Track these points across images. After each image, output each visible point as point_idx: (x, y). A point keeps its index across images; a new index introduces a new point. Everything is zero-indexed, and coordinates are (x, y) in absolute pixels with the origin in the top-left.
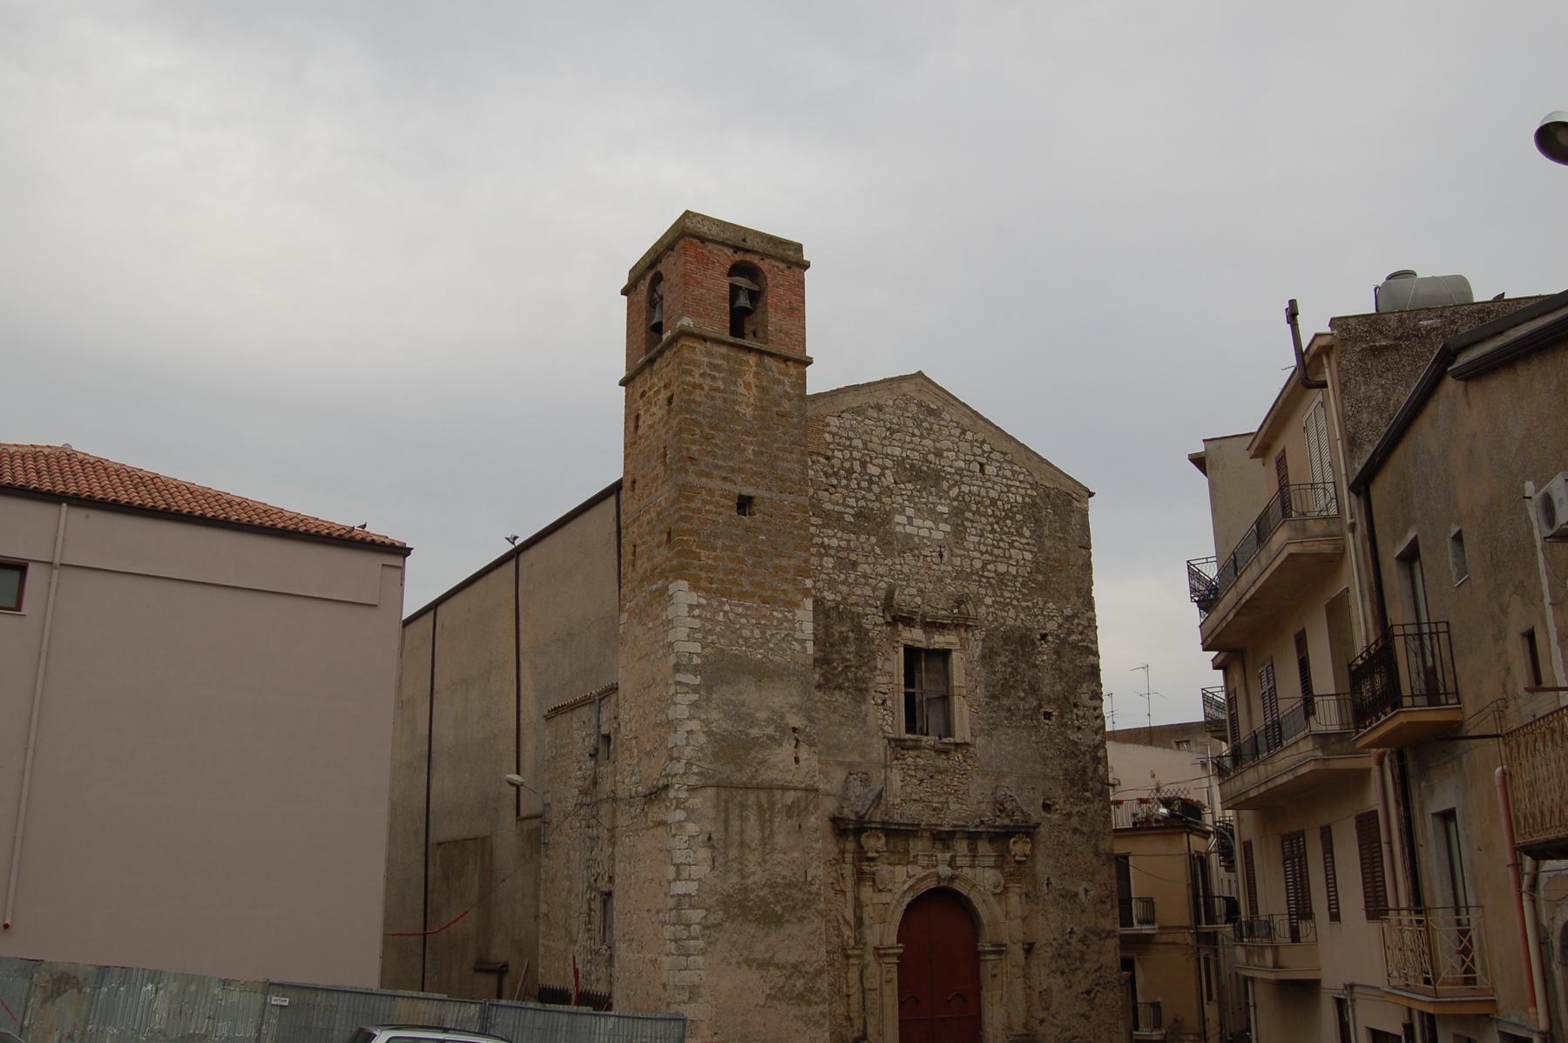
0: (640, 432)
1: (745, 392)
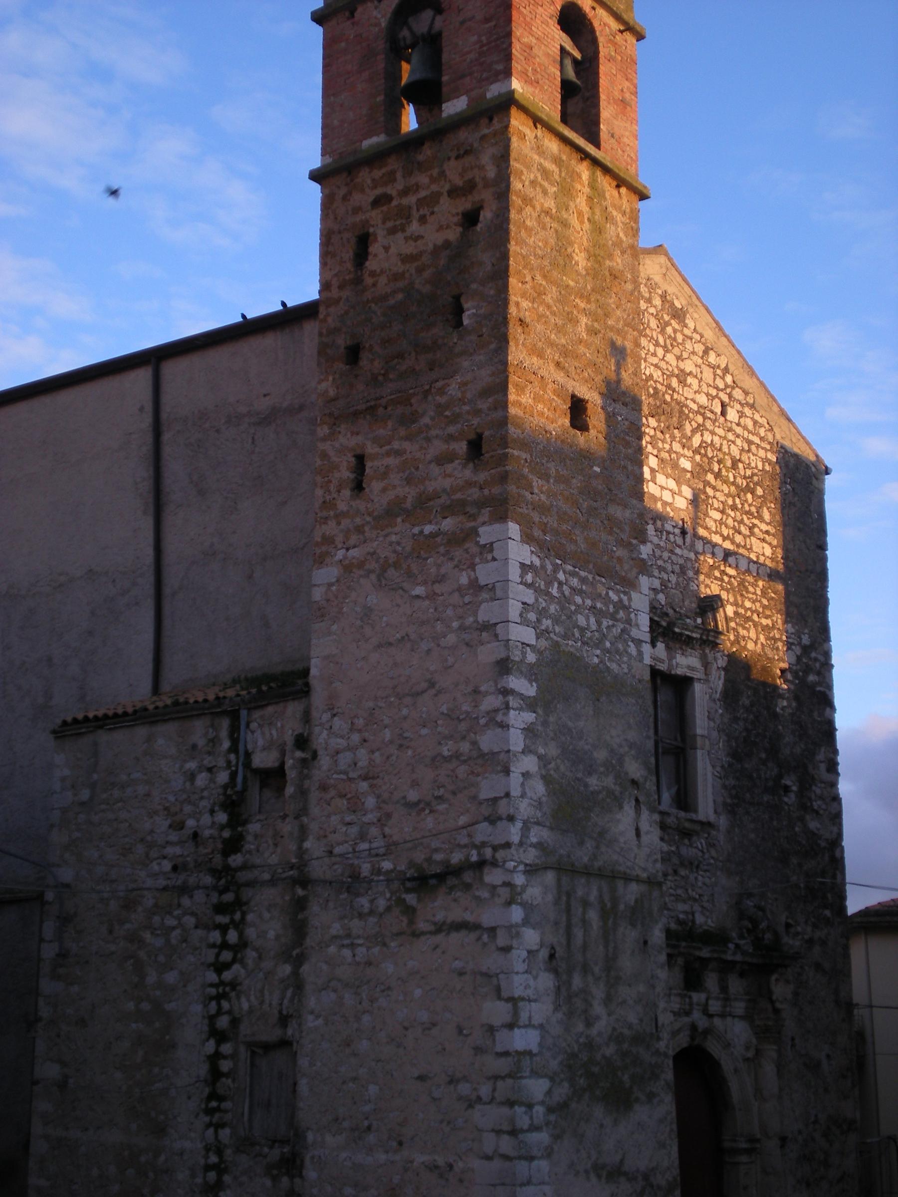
0: (371, 264)
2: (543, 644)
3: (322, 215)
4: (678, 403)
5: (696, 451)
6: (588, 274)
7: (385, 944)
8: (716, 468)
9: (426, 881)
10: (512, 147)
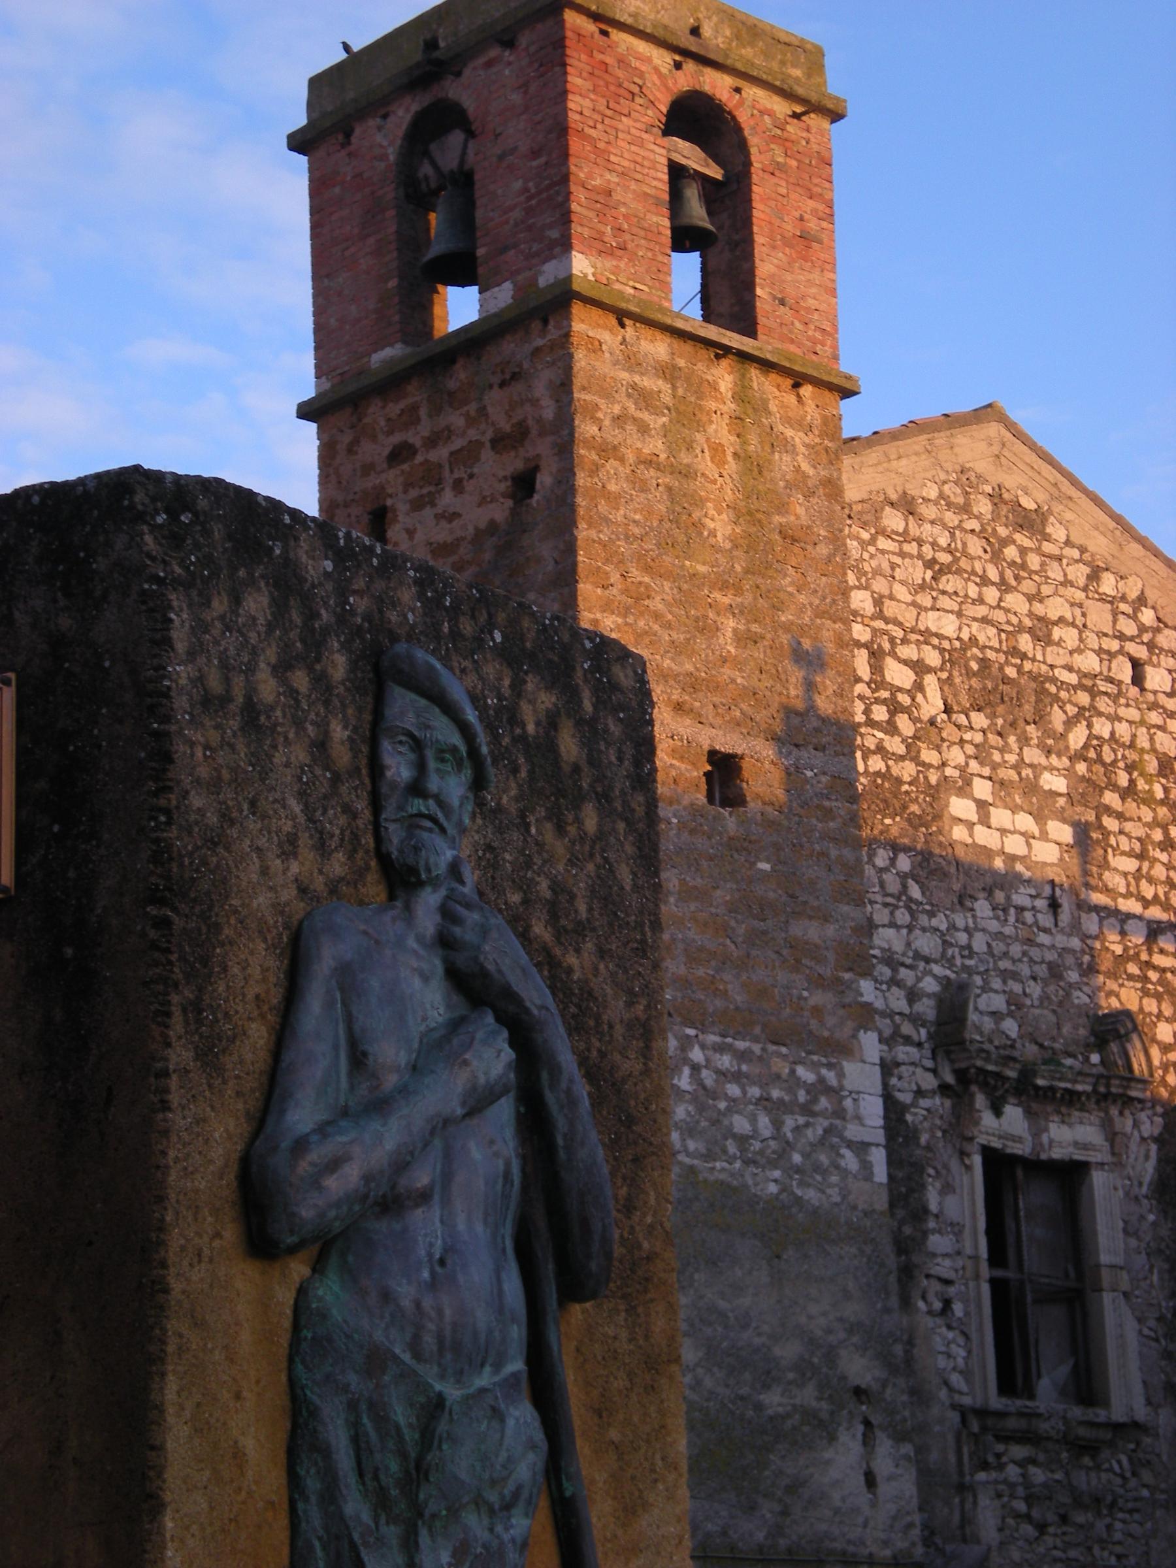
1: (710, 469)
3: (320, 476)
4: (1034, 677)
5: (1080, 756)
8: (1123, 779)
10: (575, 369)
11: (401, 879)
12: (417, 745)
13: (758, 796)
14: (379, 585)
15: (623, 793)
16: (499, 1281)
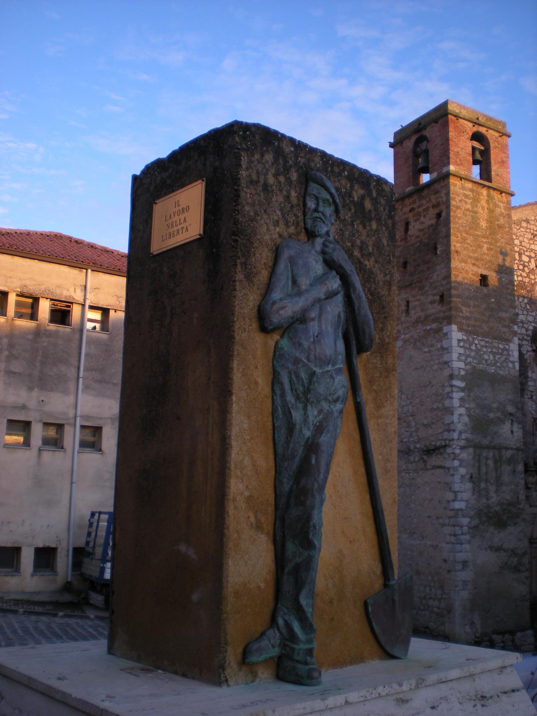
0: (410, 233)
2: (468, 367)
6: (487, 228)
7: (418, 473)
9: (430, 451)
11: (311, 235)
12: (317, 199)
13: (492, 284)
14: (308, 156)
15: (385, 219)
16: (335, 344)
